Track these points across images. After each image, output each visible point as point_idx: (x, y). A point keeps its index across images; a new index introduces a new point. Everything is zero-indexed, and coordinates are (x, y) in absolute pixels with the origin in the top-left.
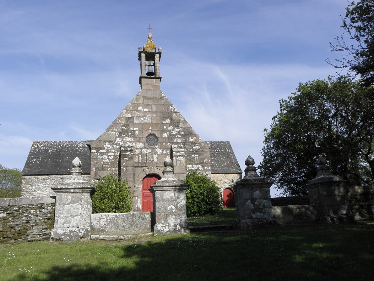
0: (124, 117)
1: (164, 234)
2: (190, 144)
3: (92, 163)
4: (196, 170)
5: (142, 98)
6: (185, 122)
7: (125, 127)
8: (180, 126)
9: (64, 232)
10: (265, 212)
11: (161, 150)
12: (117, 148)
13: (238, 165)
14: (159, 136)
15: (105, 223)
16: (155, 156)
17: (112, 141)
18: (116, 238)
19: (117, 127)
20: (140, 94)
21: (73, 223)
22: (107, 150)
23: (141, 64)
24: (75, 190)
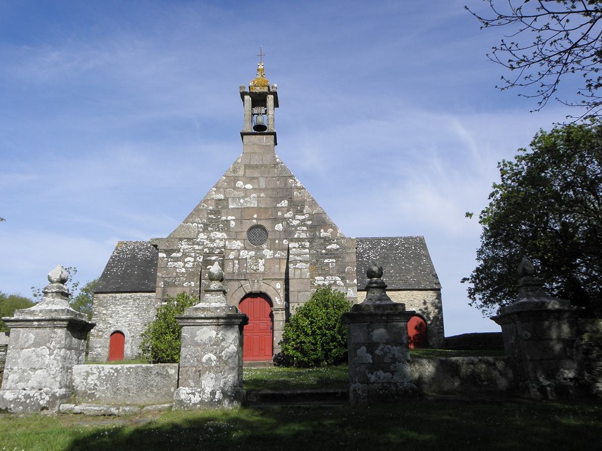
0: (213, 199)
1: (189, 409)
2: (322, 241)
3: (158, 274)
4: (330, 285)
5: (242, 168)
6: (313, 204)
7: (214, 214)
8: (305, 211)
9: (16, 396)
10: (396, 371)
11: (272, 252)
12: (200, 250)
13: (434, 276)
14: (268, 228)
15: (96, 382)
16: (261, 262)
17: (192, 239)
18: (102, 411)
19: (201, 216)
20: (239, 161)
21: (33, 383)
22: (183, 253)
24: (40, 323)
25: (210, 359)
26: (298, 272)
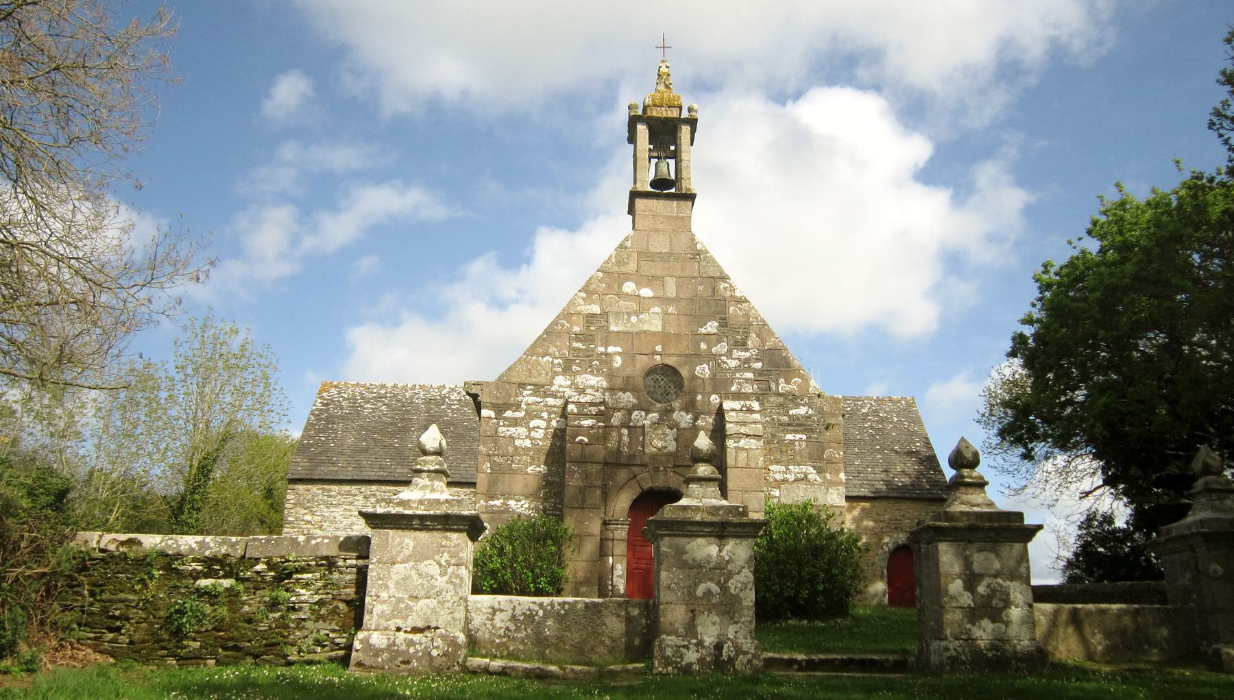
0: (579, 313)
2: (781, 399)
8: (749, 342)
17: (543, 386)
22: (526, 411)
23: (635, 155)
25: (708, 592)
26: (742, 456)
